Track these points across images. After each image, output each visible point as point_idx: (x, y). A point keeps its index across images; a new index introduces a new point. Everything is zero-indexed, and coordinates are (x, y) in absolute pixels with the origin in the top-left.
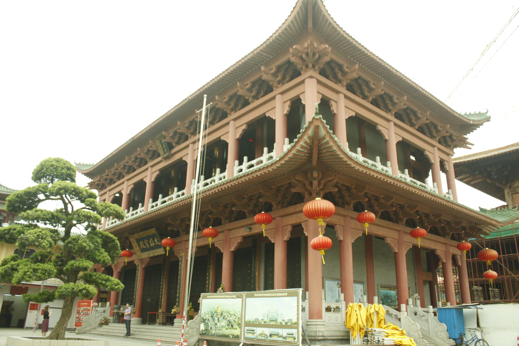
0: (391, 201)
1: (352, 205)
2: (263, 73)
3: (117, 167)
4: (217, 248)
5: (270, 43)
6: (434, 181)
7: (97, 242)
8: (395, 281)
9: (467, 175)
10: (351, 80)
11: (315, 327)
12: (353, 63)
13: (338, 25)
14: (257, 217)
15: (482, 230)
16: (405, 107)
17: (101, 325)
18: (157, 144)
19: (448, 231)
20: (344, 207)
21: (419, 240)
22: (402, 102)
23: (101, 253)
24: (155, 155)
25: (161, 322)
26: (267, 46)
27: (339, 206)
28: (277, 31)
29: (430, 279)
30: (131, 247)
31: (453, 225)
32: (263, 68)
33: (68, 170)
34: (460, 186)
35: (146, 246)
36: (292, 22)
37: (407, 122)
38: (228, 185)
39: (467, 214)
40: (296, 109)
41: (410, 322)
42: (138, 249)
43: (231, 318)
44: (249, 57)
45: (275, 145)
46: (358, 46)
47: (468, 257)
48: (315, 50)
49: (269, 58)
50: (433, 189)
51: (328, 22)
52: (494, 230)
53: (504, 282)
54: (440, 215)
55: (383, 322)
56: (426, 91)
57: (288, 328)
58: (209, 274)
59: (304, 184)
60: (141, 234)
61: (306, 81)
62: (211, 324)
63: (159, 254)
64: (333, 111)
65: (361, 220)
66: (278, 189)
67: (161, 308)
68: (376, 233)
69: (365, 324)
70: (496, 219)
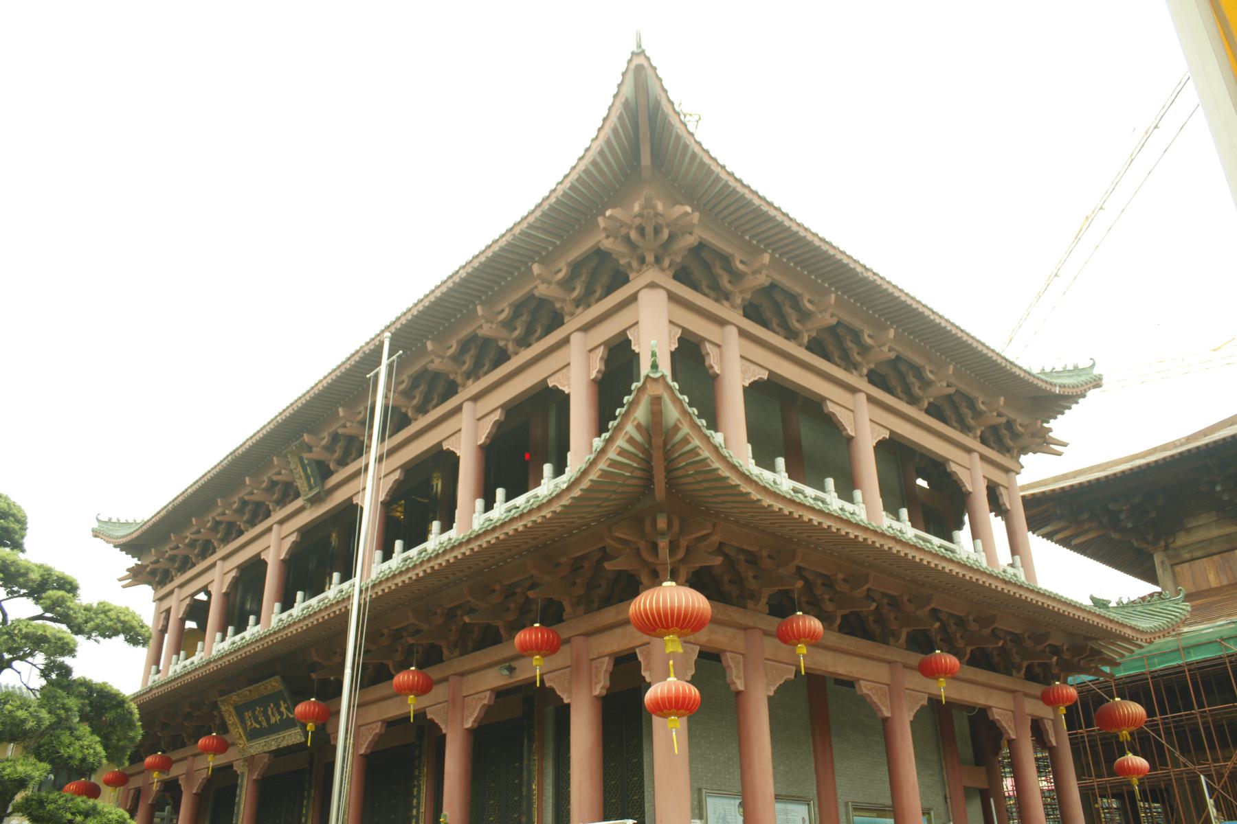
0: (865, 588)
1: (764, 600)
4: (432, 721)
5: (551, 208)
6: (975, 535)
7: (64, 707)
9: (1061, 524)
10: (877, 364)
12: (756, 252)
13: (715, 160)
14: (521, 637)
16: (892, 355)
18: (292, 466)
19: (1017, 659)
20: (745, 607)
23: (78, 739)
24: (288, 492)
26: (544, 214)
27: (732, 604)
28: (566, 176)
29: (983, 784)
30: (223, 729)
31: (1029, 643)
32: (536, 269)
34: (1041, 549)
35: (260, 723)
36: (601, 153)
38: (447, 557)
40: (620, 364)
42: (241, 731)
44: (502, 243)
46: (765, 208)
47: (1071, 725)
48: (661, 221)
49: (553, 244)
50: (973, 556)
52: (1132, 651)
53: (1171, 784)
56: (941, 317)
58: (419, 792)
59: (638, 549)
60: (245, 691)
61: (641, 295)
63: (290, 743)
64: (712, 367)
66: (576, 566)
68: (831, 669)
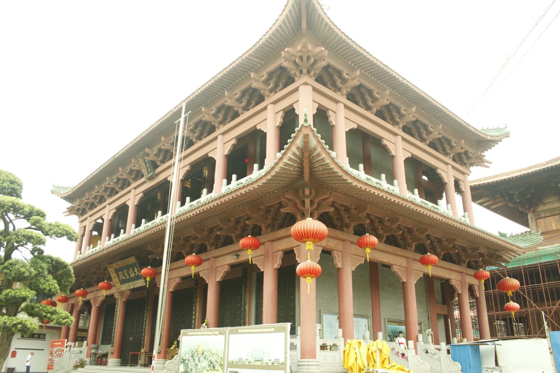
0: (397, 224)
1: (352, 228)
2: (253, 81)
3: (98, 190)
4: (202, 278)
6: (448, 203)
8: (404, 315)
9: (487, 199)
10: (381, 107)
11: (307, 367)
12: (353, 69)
14: (243, 241)
15: (501, 257)
16: (414, 119)
17: (76, 367)
18: (140, 163)
19: (464, 258)
21: (430, 267)
22: (410, 114)
24: (138, 175)
25: (143, 363)
26: (256, 50)
27: (337, 229)
29: (445, 313)
30: (110, 279)
32: (252, 75)
33: (11, 183)
35: (126, 277)
36: (284, 21)
37: (417, 137)
38: (210, 205)
39: (483, 239)
41: (418, 361)
43: (213, 358)
45: (266, 160)
48: (310, 54)
50: (447, 212)
51: (324, 23)
52: (516, 257)
54: (454, 240)
55: (387, 361)
57: (275, 369)
58: (196, 309)
60: (119, 263)
61: (300, 88)
62: (191, 364)
63: (139, 286)
64: (331, 122)
65: (362, 245)
66: (268, 210)
67: (143, 347)
68: (381, 260)
69: (366, 365)
70: (517, 244)
